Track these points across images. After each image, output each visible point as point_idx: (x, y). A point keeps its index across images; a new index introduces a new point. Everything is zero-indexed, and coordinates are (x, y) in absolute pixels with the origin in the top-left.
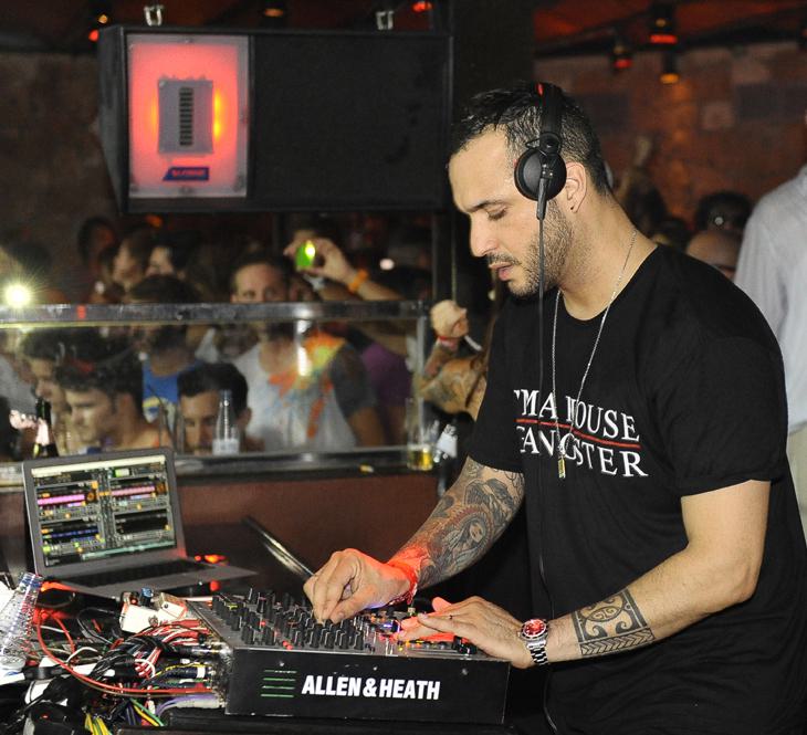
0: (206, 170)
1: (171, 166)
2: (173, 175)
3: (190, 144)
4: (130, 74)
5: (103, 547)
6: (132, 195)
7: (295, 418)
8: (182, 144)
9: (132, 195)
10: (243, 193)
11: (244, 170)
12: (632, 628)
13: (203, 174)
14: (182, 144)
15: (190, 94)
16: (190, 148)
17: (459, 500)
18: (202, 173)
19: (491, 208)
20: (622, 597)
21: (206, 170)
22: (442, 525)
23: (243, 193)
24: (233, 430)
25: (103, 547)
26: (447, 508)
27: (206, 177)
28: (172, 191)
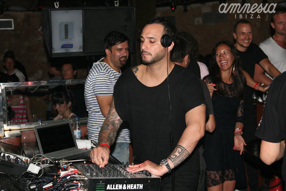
0: (72, 45)
1: (63, 44)
2: (63, 47)
3: (67, 38)
4: (52, 21)
5: (69, 167)
6: (53, 52)
7: (174, 63)
8: (65, 38)
9: (53, 52)
10: (82, 50)
11: (82, 44)
12: (182, 151)
13: (71, 46)
14: (65, 38)
15: (67, 25)
16: (68, 39)
17: (110, 125)
18: (71, 46)
19: (151, 39)
20: (179, 147)
21: (72, 45)
22: (108, 132)
23: (82, 50)
24: (26, 152)
25: (69, 167)
26: (108, 127)
27: (72, 47)
28: (63, 51)
